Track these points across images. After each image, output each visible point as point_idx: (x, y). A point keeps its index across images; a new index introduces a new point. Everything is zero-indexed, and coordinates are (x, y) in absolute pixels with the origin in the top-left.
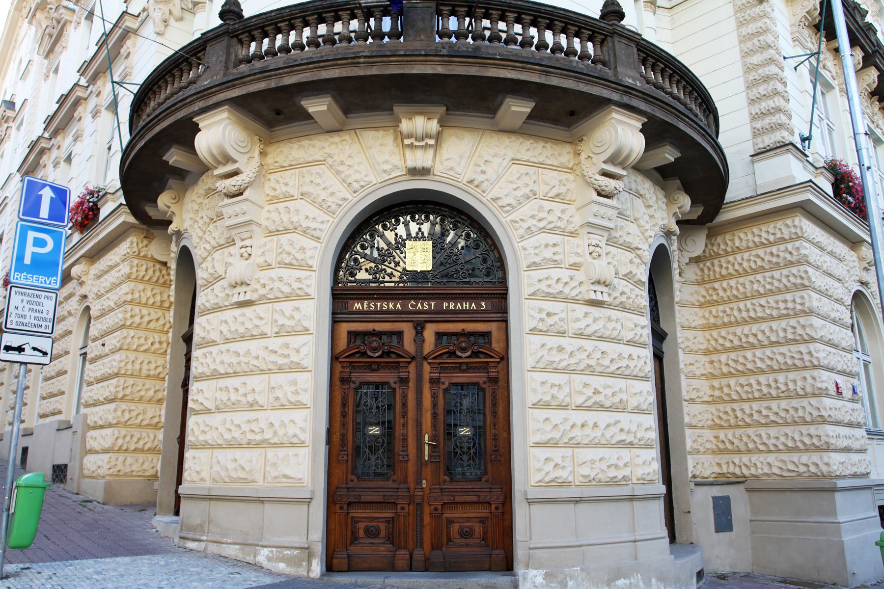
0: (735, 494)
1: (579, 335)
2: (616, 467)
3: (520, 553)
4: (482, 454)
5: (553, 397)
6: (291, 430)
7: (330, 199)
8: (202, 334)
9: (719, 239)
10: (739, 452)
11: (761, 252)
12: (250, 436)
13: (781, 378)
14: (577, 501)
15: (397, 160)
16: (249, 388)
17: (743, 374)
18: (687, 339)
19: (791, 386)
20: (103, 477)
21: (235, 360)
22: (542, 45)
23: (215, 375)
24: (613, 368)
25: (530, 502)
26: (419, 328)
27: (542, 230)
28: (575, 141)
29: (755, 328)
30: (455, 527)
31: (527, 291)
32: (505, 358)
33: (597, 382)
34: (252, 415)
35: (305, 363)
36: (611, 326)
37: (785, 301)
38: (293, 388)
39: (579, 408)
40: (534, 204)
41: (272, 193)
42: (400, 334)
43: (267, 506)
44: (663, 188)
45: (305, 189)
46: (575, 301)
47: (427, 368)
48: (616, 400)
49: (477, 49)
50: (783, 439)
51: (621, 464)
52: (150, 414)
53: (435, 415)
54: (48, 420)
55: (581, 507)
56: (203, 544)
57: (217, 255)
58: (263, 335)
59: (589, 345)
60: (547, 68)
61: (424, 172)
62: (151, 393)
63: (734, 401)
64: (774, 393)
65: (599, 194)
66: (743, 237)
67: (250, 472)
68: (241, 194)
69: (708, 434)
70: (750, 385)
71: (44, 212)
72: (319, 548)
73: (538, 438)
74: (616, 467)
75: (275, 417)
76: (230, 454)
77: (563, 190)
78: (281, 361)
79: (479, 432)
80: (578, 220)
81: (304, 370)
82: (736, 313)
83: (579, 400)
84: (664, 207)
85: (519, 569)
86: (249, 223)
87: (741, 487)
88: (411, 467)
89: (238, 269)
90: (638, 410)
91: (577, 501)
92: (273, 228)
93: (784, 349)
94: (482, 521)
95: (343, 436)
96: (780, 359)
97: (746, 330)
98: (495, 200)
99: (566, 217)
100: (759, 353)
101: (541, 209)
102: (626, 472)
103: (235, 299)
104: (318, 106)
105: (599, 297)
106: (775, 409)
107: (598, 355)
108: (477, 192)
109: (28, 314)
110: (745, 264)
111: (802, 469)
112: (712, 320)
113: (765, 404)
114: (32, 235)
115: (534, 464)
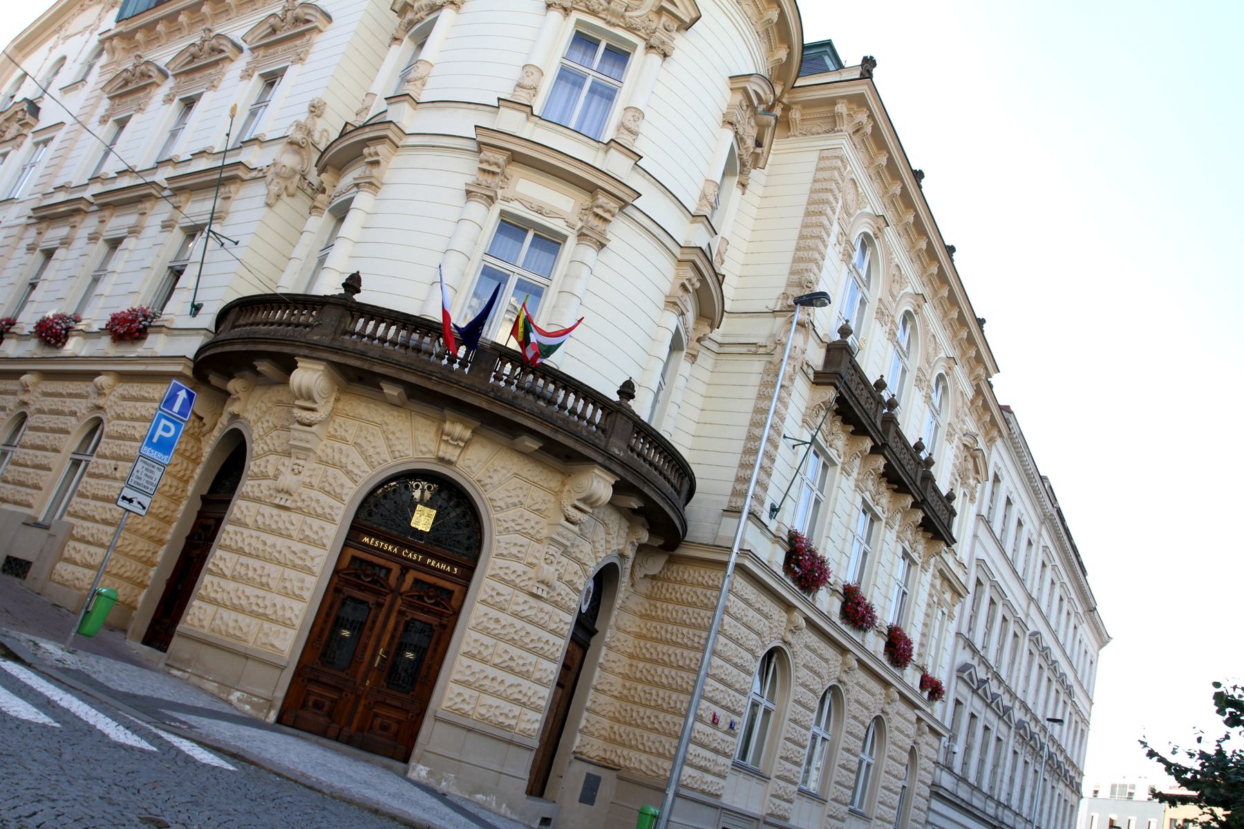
0: (607, 777)
1: (515, 615)
2: (507, 716)
3: (417, 751)
4: (414, 677)
5: (480, 652)
6: (288, 614)
7: (376, 457)
8: (238, 516)
9: (675, 567)
10: (624, 745)
11: (699, 591)
12: (255, 608)
13: (674, 696)
14: (470, 730)
15: (433, 446)
16: (266, 572)
17: (650, 683)
18: (618, 640)
19: (678, 705)
20: (79, 589)
21: (261, 547)
22: (563, 406)
24: (531, 646)
25: (437, 719)
26: (405, 570)
27: (516, 532)
28: (567, 474)
29: (672, 650)
30: (378, 721)
31: (489, 572)
32: (456, 614)
33: (515, 652)
35: (315, 569)
36: (541, 615)
37: (700, 637)
38: (300, 585)
39: (495, 666)
40: (518, 511)
41: (333, 432)
42: (389, 570)
43: (250, 663)
44: (629, 521)
45: (359, 441)
46: (521, 589)
47: (399, 601)
48: (524, 669)
49: (515, 397)
50: (657, 744)
51: (511, 715)
52: (138, 547)
53: (393, 637)
55: (471, 735)
56: (187, 675)
57: (272, 458)
58: (290, 537)
59: (519, 624)
60: (557, 428)
61: (449, 463)
62: (147, 528)
63: (635, 703)
64: (665, 706)
65: (567, 520)
67: (246, 634)
68: (310, 425)
69: (606, 723)
70: (651, 694)
71: (176, 408)
72: (279, 704)
73: (458, 677)
74: (507, 716)
75: (279, 600)
76: (234, 615)
77: (543, 507)
78: (297, 561)
79: (419, 661)
80: (545, 533)
81: (312, 574)
82: (663, 632)
83: (498, 660)
84: (624, 535)
85: (412, 763)
86: (309, 450)
87: (614, 774)
88: (363, 668)
89: (287, 480)
90: (539, 682)
91: (470, 730)
92: (324, 459)
93: (684, 674)
94: (399, 722)
95: (322, 630)
96: (679, 680)
97: (665, 649)
98: (491, 500)
99: (537, 527)
100: (666, 671)
101: (521, 516)
102: (513, 722)
103: (277, 501)
104: (391, 391)
105: (539, 593)
106: (661, 719)
107: (523, 633)
108: (481, 490)
109: (143, 477)
110: (685, 596)
111: (662, 772)
112: (644, 632)
113: (656, 713)
114: (164, 422)
115: (449, 694)
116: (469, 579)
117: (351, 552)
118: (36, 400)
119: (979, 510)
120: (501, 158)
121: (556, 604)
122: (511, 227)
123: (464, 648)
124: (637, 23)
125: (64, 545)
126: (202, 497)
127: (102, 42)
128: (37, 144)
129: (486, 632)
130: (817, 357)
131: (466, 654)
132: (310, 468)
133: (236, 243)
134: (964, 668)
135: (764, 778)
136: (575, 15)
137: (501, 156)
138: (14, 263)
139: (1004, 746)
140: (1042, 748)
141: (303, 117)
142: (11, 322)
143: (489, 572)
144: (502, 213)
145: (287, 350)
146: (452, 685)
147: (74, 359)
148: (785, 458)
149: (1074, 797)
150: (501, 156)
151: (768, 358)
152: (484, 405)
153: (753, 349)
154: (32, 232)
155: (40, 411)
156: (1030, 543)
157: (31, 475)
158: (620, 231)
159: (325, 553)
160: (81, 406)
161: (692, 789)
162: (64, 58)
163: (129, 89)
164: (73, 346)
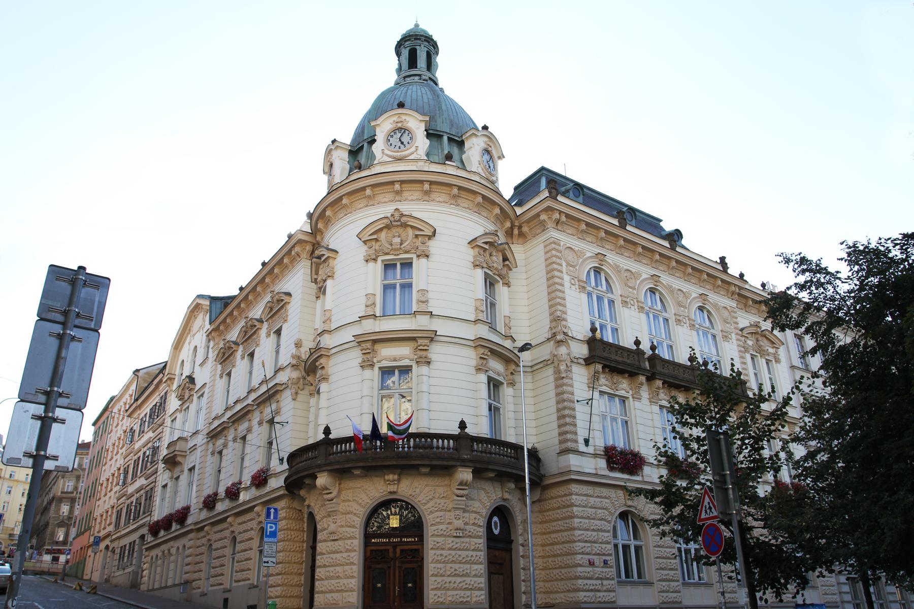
1: (450, 549)
15: (384, 488)
23: (325, 566)
26: (395, 547)
33: (457, 566)
34: (337, 581)
46: (449, 536)
54: (241, 583)
58: (341, 552)
59: (453, 553)
61: (394, 493)
66: (554, 492)
75: (345, 581)
79: (414, 587)
80: (450, 506)
89: (332, 527)
102: (468, 599)
104: (357, 472)
116: (423, 541)
117: (369, 548)
118: (238, 529)
120: (369, 345)
121: (470, 536)
122: (387, 372)
123: (431, 573)
124: (408, 248)
125: (266, 592)
127: (208, 336)
128: (199, 398)
129: (438, 562)
130: (583, 351)
131: (432, 575)
132: (340, 518)
135: (649, 584)
136: (380, 259)
138: (208, 463)
141: (294, 350)
142: (216, 494)
143: (430, 534)
144: (380, 368)
145: (311, 472)
146: (431, 592)
147: (244, 503)
148: (581, 412)
150: (370, 344)
151: (552, 365)
152: (395, 463)
153: (545, 363)
154: (211, 445)
155: (240, 533)
157: (244, 565)
158: (437, 352)
159: (357, 553)
160: (254, 524)
161: (590, 603)
162: (196, 347)
163: (226, 357)
164: (243, 497)
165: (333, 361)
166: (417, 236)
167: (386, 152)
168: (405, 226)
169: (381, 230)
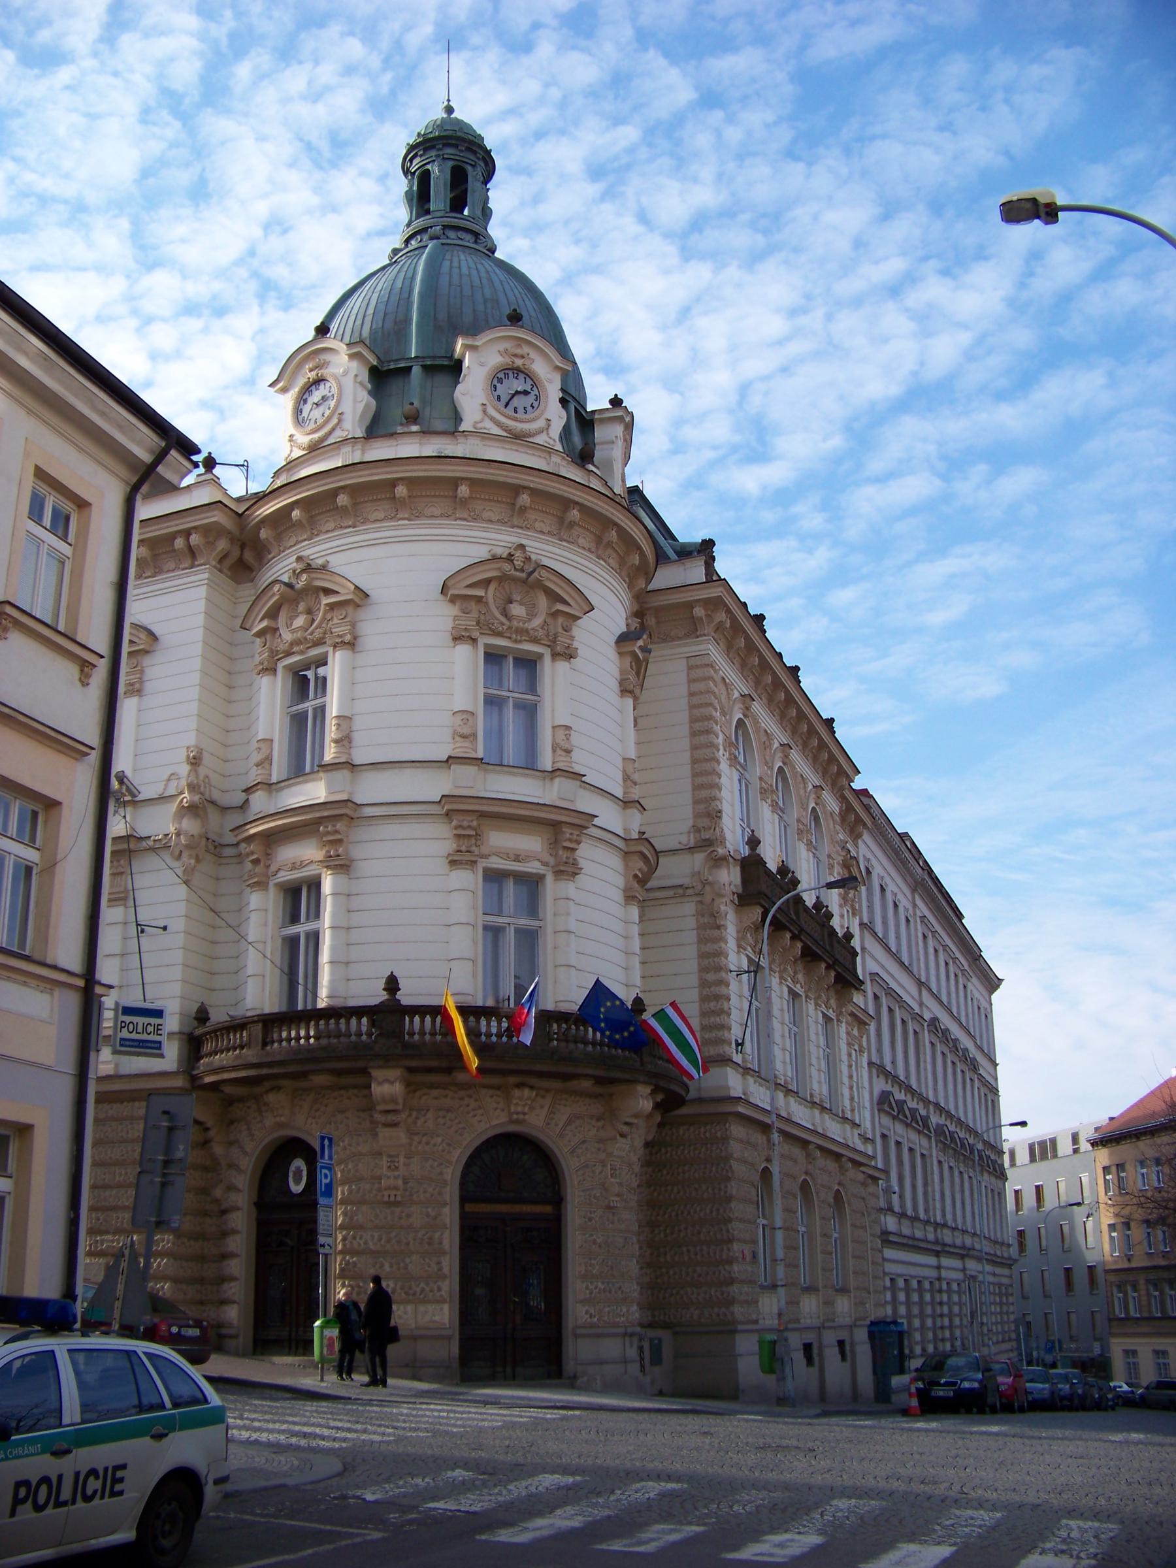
119: (861, 919)
122: (494, 877)
126: (255, 1204)
133: (165, 928)
134: (884, 1098)
137: (469, 819)
139: (928, 1161)
140: (972, 1152)
149: (999, 1183)
151: (698, 899)
156: (908, 921)
165: (360, 832)
166: (555, 614)
167: (491, 411)
168: (540, 586)
169: (487, 582)
